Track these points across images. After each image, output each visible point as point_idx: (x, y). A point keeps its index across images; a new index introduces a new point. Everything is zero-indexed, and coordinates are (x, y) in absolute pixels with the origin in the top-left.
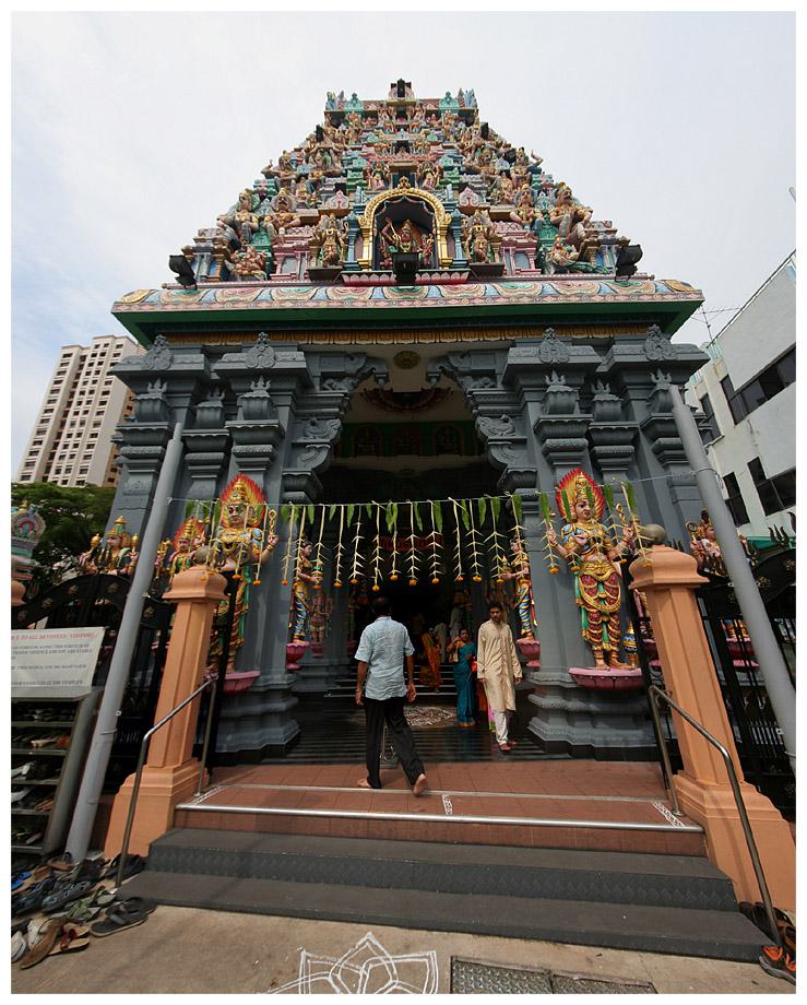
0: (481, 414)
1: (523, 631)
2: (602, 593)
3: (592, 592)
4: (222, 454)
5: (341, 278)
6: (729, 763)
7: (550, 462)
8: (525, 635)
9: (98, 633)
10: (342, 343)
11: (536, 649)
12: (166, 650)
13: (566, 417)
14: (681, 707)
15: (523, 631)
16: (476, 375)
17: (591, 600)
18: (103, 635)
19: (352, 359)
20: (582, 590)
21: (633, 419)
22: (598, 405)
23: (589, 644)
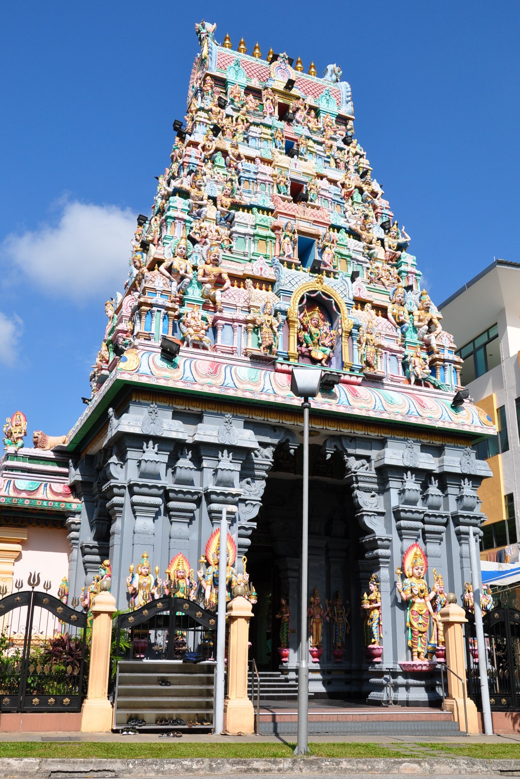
0: (358, 488)
1: (373, 640)
2: (421, 620)
3: (417, 620)
4: (256, 524)
5: (274, 364)
6: (463, 685)
7: (400, 535)
8: (374, 643)
9: (27, 607)
10: (273, 421)
11: (381, 651)
12: (475, 626)
13: (413, 508)
14: (451, 669)
15: (373, 640)
16: (358, 457)
17: (415, 624)
18: (45, 611)
19: (275, 431)
20: (411, 618)
21: (448, 510)
22: (430, 497)
23: (410, 649)
